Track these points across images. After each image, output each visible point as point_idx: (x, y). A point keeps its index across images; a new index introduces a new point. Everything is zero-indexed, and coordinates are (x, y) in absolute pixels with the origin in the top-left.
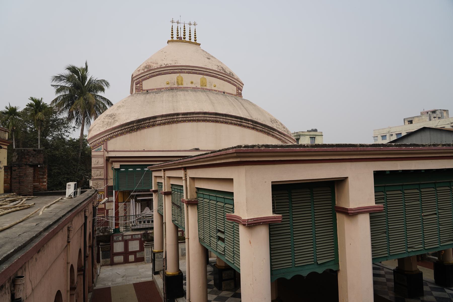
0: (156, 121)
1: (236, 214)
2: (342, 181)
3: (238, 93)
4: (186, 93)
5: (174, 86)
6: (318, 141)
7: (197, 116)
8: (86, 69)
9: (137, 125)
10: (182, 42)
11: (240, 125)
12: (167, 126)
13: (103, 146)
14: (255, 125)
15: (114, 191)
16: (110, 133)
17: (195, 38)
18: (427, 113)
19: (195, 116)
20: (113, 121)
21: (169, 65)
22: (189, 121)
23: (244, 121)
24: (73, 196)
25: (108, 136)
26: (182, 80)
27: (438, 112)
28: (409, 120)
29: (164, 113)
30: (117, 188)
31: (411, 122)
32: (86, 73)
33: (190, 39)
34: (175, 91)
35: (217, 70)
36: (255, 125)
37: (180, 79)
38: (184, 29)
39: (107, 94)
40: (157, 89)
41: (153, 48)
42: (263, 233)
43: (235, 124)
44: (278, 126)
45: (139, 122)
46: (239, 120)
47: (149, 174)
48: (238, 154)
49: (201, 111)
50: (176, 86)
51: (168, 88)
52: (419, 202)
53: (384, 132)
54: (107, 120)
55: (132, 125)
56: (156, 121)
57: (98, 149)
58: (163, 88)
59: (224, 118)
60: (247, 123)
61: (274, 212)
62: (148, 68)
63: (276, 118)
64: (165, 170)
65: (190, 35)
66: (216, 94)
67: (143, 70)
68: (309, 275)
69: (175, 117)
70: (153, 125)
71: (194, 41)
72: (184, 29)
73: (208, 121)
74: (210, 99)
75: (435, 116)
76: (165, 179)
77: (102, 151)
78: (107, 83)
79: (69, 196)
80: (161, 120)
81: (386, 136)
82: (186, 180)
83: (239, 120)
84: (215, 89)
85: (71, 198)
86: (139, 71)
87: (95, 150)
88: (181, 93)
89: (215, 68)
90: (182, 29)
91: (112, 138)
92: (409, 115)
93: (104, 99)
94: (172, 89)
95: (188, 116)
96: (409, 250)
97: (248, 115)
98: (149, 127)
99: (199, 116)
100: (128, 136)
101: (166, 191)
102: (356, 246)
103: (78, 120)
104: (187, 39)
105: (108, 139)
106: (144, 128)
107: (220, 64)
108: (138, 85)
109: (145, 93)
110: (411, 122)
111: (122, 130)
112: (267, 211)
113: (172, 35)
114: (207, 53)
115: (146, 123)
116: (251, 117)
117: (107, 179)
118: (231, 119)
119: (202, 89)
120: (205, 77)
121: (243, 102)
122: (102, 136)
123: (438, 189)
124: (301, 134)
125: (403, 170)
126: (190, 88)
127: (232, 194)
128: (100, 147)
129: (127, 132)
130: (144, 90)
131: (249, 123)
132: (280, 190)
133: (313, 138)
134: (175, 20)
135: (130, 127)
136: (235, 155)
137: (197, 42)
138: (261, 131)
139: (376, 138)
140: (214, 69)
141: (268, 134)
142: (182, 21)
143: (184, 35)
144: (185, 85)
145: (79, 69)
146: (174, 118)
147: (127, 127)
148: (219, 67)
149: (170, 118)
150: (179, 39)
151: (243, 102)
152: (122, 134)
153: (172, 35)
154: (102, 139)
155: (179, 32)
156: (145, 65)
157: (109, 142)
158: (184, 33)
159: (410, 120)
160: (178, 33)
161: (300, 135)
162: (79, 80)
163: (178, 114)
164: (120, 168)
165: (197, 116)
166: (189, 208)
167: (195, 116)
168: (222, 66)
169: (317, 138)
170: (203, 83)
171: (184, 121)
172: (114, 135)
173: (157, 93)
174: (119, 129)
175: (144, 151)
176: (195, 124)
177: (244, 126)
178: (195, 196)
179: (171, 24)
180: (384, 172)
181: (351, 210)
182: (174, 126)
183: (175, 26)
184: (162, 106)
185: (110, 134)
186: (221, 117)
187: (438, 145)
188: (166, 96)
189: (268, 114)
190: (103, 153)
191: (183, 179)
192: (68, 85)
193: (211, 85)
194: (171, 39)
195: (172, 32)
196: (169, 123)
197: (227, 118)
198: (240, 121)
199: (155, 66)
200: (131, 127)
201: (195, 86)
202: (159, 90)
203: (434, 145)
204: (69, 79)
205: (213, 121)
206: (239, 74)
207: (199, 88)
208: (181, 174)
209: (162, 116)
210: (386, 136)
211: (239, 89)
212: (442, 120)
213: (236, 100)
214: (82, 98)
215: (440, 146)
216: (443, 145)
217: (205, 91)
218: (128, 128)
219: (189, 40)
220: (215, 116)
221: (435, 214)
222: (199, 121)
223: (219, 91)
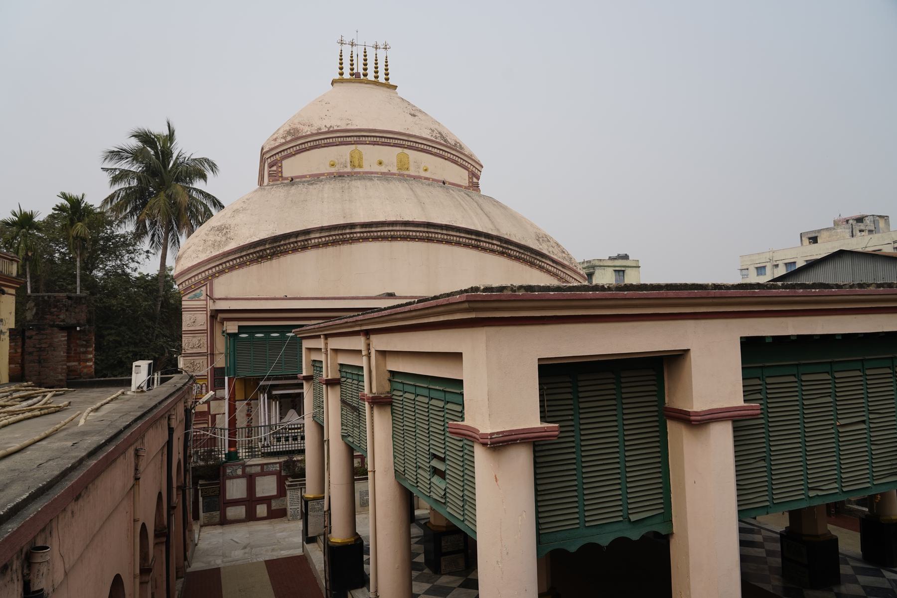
0: (310, 239)
1: (468, 422)
2: (674, 360)
3: (472, 182)
4: (369, 183)
6: (631, 278)
7: (390, 228)
8: (171, 136)
9: (272, 248)
10: (361, 82)
11: (476, 247)
12: (330, 250)
13: (204, 288)
14: (506, 248)
15: (226, 378)
16: (218, 263)
17: (387, 74)
18: (847, 221)
19: (387, 229)
20: (224, 239)
21: (336, 128)
22: (375, 239)
23: (483, 239)
24: (145, 389)
25: (214, 270)
26: (361, 158)
27: (867, 221)
29: (326, 224)
30: (232, 372)
31: (814, 240)
32: (171, 144)
33: (377, 77)
34: (347, 179)
35: (429, 137)
36: (506, 248)
37: (357, 156)
38: (365, 56)
39: (210, 185)
40: (311, 176)
41: (304, 94)
42: (521, 460)
43: (466, 245)
44: (551, 249)
45: (276, 242)
46: (473, 237)
47: (296, 344)
48: (472, 305)
49: (399, 219)
51: (332, 173)
53: (761, 260)
55: (262, 248)
56: (310, 239)
57: (195, 296)
58: (323, 174)
59: (444, 232)
60: (489, 243)
61: (543, 418)
62: (294, 134)
64: (326, 337)
65: (376, 68)
67: (284, 138)
69: (348, 231)
70: (304, 248)
71: (384, 81)
72: (365, 56)
73: (413, 239)
74: (416, 195)
75: (862, 227)
76: (327, 355)
77: (202, 298)
79: (138, 388)
80: (320, 238)
83: (473, 237)
85: (142, 391)
86: (275, 140)
87: (188, 296)
88: (358, 183)
89: (426, 134)
90: (361, 57)
91: (222, 272)
92: (811, 227)
93: (207, 196)
94: (340, 176)
95: (373, 229)
96: (812, 494)
97: (491, 226)
98: (295, 250)
99: (395, 228)
100: (254, 268)
101: (329, 377)
103: (156, 238)
104: (371, 77)
105: (213, 276)
106: (285, 252)
107: (437, 126)
108: (274, 168)
109: (287, 185)
111: (241, 257)
112: (529, 417)
113: (341, 69)
114: (409, 104)
115: (289, 244)
116: (498, 230)
117: (212, 354)
118: (458, 234)
119: (400, 175)
120: (406, 151)
121: (480, 201)
122: (203, 269)
123: (868, 372)
124: (597, 263)
125: (798, 336)
126: (377, 173)
128: (198, 291)
129: (252, 261)
130: (286, 179)
131: (495, 242)
132: (555, 376)
133: (620, 272)
134: (347, 40)
135: (258, 252)
136: (466, 305)
137: (391, 82)
138: (517, 259)
139: (745, 272)
140: (424, 136)
141: (532, 264)
142: (359, 41)
143: (365, 69)
144: (366, 168)
146: (345, 234)
147: (252, 251)
148: (433, 131)
149: (336, 233)
150: (357, 75)
151: (480, 201)
152: (241, 265)
153: (341, 69)
154: (203, 274)
156: (288, 128)
158: (365, 65)
159: (813, 235)
160: (352, 65)
161: (594, 267)
162: (158, 158)
163: (352, 226)
164: (239, 333)
165: (390, 228)
167: (387, 229)
168: (440, 129)
169: (628, 272)
170: (403, 164)
171: (365, 239)
172: (226, 267)
173: (312, 184)
175: (286, 298)
176: (386, 245)
177: (484, 249)
178: (387, 387)
179: (339, 47)
180: (762, 338)
181: (697, 414)
182: (345, 248)
183: (347, 50)
184: (321, 209)
185: (218, 266)
186: (439, 231)
187: (869, 285)
188: (328, 189)
189: (532, 225)
191: (364, 353)
192: (136, 168)
193: (419, 168)
194: (338, 77)
195: (341, 64)
196: (334, 243)
197: (451, 233)
198: (475, 240)
199: (307, 130)
202: (316, 178)
203: (861, 286)
204: (136, 155)
205: (421, 239)
206: (473, 146)
207: (394, 174)
208: (358, 343)
209: (322, 229)
210: (764, 267)
211: (474, 176)
212: (875, 237)
213: (468, 198)
215: (872, 288)
217: (406, 180)
219: (373, 79)
220: (426, 230)
221: (863, 422)
222: (393, 238)
223: (434, 180)
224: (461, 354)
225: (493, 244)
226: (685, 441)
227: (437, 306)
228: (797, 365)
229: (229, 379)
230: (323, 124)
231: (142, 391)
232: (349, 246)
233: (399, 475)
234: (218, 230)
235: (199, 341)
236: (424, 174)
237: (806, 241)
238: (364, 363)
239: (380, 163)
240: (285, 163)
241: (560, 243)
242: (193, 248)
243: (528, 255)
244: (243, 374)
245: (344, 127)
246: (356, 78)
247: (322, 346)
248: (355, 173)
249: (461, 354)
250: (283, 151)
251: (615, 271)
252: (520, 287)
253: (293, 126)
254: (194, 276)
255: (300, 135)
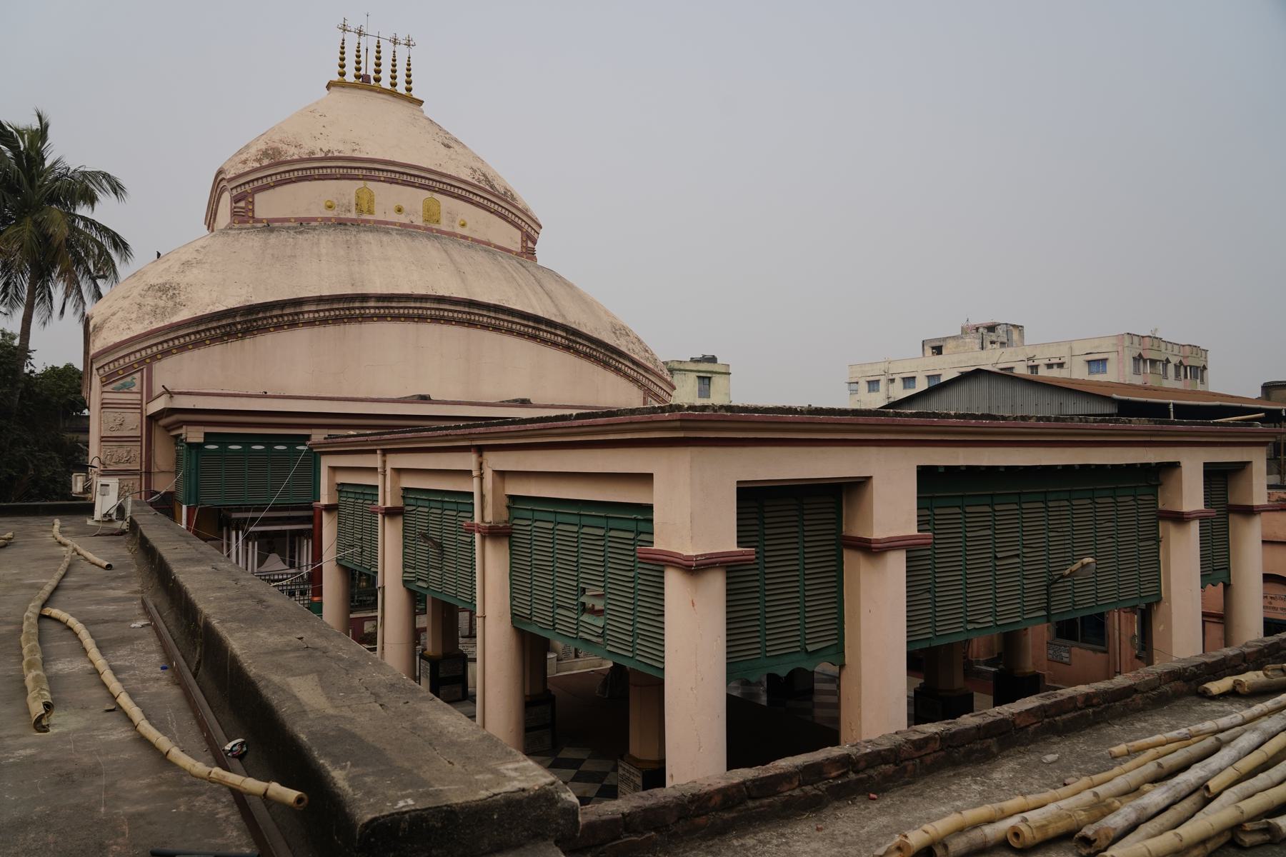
0: (303, 313)
1: (658, 545)
2: (857, 486)
3: (527, 247)
4: (385, 239)
5: (349, 215)
7: (418, 305)
8: (41, 134)
9: (245, 322)
10: (372, 89)
11: (534, 338)
12: (331, 330)
13: (138, 375)
15: (184, 507)
16: (161, 339)
17: (409, 83)
18: (977, 329)
19: (413, 305)
20: (170, 304)
21: (336, 154)
24: (114, 517)
25: (155, 349)
26: (371, 201)
27: (1000, 330)
28: (934, 344)
30: (193, 499)
32: (43, 144)
33: (394, 85)
34: (353, 230)
35: (470, 180)
37: (366, 197)
38: (379, 52)
39: (105, 211)
40: (296, 220)
41: (286, 100)
42: (716, 584)
43: (520, 335)
44: (631, 346)
45: (251, 314)
46: (531, 324)
47: (313, 459)
49: (430, 292)
50: (353, 215)
51: (329, 219)
52: (989, 532)
54: (150, 301)
55: (230, 321)
56: (303, 313)
57: (124, 385)
58: (315, 219)
59: (492, 314)
61: (739, 544)
62: (272, 156)
63: (627, 324)
65: (394, 71)
66: (469, 246)
67: (259, 160)
68: (792, 673)
69: (357, 304)
70: (293, 325)
71: (404, 92)
72: (379, 52)
73: (448, 321)
75: (994, 339)
76: (385, 476)
77: (134, 389)
78: (118, 185)
79: (105, 515)
80: (317, 311)
81: (878, 381)
82: (481, 477)
83: (531, 324)
84: (465, 232)
85: (111, 521)
86: (244, 162)
87: (113, 385)
89: (465, 174)
90: (372, 54)
91: (166, 353)
92: (936, 332)
94: (341, 223)
95: (394, 304)
96: (970, 627)
97: (554, 310)
98: (278, 327)
99: (424, 305)
100: (217, 350)
101: (388, 505)
102: (880, 612)
103: (11, 290)
104: (385, 83)
105: (154, 358)
106: (264, 330)
107: (479, 165)
108: (242, 204)
109: (262, 230)
110: (938, 350)
111: (198, 332)
112: (725, 540)
113: (342, 66)
115: (271, 317)
116: (564, 316)
117: (149, 473)
118: (510, 318)
119: (426, 229)
120: (437, 196)
121: (539, 275)
123: (1024, 506)
124: (676, 366)
126: (394, 224)
127: (649, 508)
128: (129, 379)
129: (214, 340)
130: (260, 221)
132: (752, 498)
133: (705, 380)
134: (353, 25)
135: (223, 326)
136: (678, 424)
138: (587, 356)
139: (854, 386)
140: (463, 177)
141: (606, 365)
143: (378, 72)
144: (378, 216)
145: (17, 131)
146: (354, 308)
147: (215, 324)
150: (366, 78)
151: (539, 275)
152: (197, 344)
153: (342, 66)
154: (138, 355)
155: (363, 59)
156: (264, 147)
157: (157, 366)
158: (378, 65)
159: (938, 344)
160: (358, 63)
162: (19, 163)
163: (364, 298)
164: (206, 443)
165: (418, 305)
166: (488, 545)
167: (413, 305)
168: (484, 170)
169: (716, 379)
170: (431, 214)
171: (382, 318)
172: (174, 347)
173: (301, 232)
174: (191, 330)
175: (265, 396)
176: (410, 327)
177: (544, 341)
178: (505, 515)
179: (339, 35)
180: (1072, 466)
181: (877, 541)
182: (352, 329)
183: (351, 41)
184: (318, 271)
185: (161, 343)
187: (1030, 418)
188: (326, 242)
189: (606, 312)
190: (139, 396)
191: (475, 474)
193: (453, 221)
194: (336, 78)
195: (342, 59)
196: (337, 320)
197: (501, 316)
199: (293, 153)
200: (228, 325)
201: (407, 221)
202: (303, 225)
203: (1023, 418)
205: (460, 323)
206: (528, 197)
207: (419, 227)
208: (468, 461)
209: (320, 300)
210: (878, 381)
211: (529, 238)
212: (1008, 350)
213: (522, 270)
214: (28, 219)
215: (1032, 421)
216: (1039, 419)
217: (436, 238)
218: (218, 327)
219: (389, 87)
220: (467, 310)
221: (1017, 556)
222: (422, 319)
223: (473, 240)
224: (651, 476)
225: (556, 335)
226: (862, 570)
227: (631, 423)
228: (992, 495)
229: (188, 508)
230: (320, 146)
231: (111, 521)
232: (357, 325)
233: (518, 621)
234: (160, 290)
235: (129, 452)
236: (459, 230)
237: (929, 351)
238: (474, 487)
239: (399, 210)
240: (259, 198)
241: (643, 339)
242: (120, 314)
243: (603, 354)
244: (208, 502)
245: (348, 154)
246: (364, 82)
247: (379, 464)
248: (363, 221)
249: (651, 476)
250: (257, 179)
251: (699, 377)
252: (722, 407)
253: (271, 144)
254: (123, 357)
255: (283, 158)
